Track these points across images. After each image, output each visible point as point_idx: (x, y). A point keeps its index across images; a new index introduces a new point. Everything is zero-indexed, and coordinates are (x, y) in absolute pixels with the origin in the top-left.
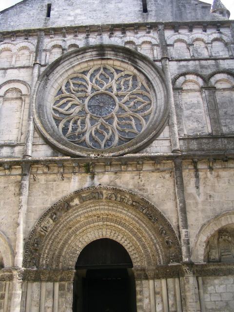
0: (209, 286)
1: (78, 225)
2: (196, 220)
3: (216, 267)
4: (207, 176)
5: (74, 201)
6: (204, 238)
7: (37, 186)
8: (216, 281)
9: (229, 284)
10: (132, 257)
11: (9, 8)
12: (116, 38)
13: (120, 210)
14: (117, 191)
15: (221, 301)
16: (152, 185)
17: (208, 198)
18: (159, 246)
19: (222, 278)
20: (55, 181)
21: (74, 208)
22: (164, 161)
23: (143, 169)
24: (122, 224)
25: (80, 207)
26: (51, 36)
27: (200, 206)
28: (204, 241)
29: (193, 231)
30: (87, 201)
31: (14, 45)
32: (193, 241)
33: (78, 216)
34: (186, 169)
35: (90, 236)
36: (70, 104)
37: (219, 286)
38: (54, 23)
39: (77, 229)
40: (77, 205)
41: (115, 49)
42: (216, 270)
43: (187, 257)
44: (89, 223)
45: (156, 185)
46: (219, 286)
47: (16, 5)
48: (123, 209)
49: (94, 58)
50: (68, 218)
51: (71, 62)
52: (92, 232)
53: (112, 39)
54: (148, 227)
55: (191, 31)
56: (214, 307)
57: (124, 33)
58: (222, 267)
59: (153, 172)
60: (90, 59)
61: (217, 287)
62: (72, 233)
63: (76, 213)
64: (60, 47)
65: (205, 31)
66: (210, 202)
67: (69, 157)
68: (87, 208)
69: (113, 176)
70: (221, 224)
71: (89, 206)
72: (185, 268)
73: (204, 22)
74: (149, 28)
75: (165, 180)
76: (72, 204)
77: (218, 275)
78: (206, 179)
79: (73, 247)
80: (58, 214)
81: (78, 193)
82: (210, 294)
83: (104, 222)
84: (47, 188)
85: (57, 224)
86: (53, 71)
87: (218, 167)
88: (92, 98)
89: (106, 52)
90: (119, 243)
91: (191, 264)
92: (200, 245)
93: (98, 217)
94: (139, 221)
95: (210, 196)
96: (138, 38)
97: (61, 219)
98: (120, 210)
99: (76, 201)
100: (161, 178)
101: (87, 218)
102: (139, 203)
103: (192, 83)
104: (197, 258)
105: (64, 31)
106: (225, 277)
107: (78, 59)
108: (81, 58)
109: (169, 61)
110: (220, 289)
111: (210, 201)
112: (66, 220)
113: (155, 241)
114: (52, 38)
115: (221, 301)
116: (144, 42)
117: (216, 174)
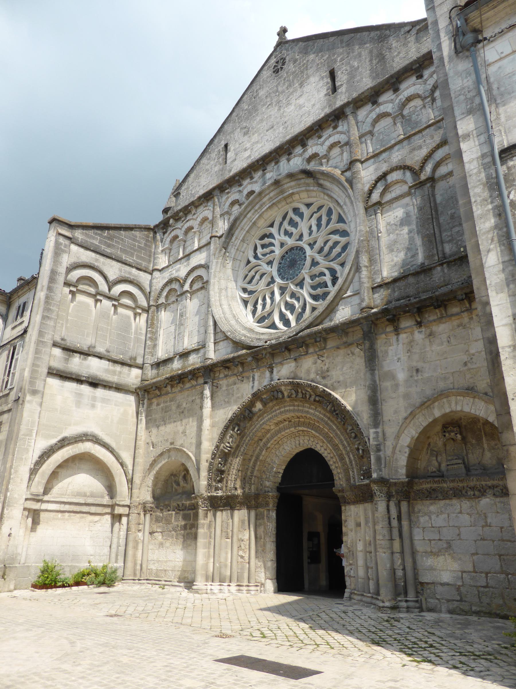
0: (422, 516)
1: (268, 435)
2: (396, 412)
3: (432, 485)
4: (413, 338)
5: (255, 407)
6: (406, 440)
7: (219, 394)
8: (432, 508)
9: (454, 513)
10: (334, 472)
11: (189, 172)
12: (296, 158)
13: (307, 409)
14: (296, 386)
15: (440, 540)
16: (338, 368)
17: (415, 374)
18: (353, 456)
19: (442, 503)
20: (235, 384)
21: (258, 414)
22: (351, 330)
23: (328, 347)
24: (315, 428)
25: (264, 413)
26: (226, 191)
27: (402, 390)
28: (406, 445)
29: (391, 430)
30: (269, 403)
31: (196, 220)
32: (391, 447)
33: (263, 423)
34: (382, 333)
35: (286, 448)
36: (257, 277)
37: (437, 516)
38: (230, 171)
39: (268, 441)
40: (260, 410)
41: (291, 176)
42: (433, 490)
43: (376, 471)
44: (279, 431)
45: (343, 368)
46: (437, 516)
47: (194, 165)
48: (309, 408)
49: (274, 201)
50: (254, 429)
51: (249, 219)
52: (288, 442)
53: (291, 162)
54: (339, 429)
55: (396, 90)
56: (429, 550)
57: (304, 145)
58: (441, 485)
59: (338, 348)
60: (270, 204)
61: (433, 517)
62: (263, 446)
63: (261, 420)
64: (404, 168)
65: (420, 77)
66: (416, 381)
67: (244, 351)
68: (272, 413)
69: (293, 364)
70: (434, 415)
71: (274, 409)
72: (375, 487)
73: (412, 64)
74: (333, 121)
75: (354, 357)
76: (255, 410)
77: (436, 498)
78: (412, 344)
79: (269, 464)
80: (242, 424)
81: (256, 396)
82: (424, 528)
83: (295, 427)
84: (228, 394)
85: (243, 437)
86: (231, 239)
87: (431, 318)
88: (283, 257)
89: (285, 186)
90: (324, 458)
91: (382, 481)
92: (400, 451)
93: (290, 421)
94: (329, 422)
95: (417, 371)
96: (322, 144)
97: (246, 431)
98: (307, 409)
99: (259, 406)
100: (349, 355)
101: (277, 424)
102: (323, 397)
103: (399, 184)
104: (397, 471)
105: (237, 178)
106: (447, 501)
107: (256, 211)
108: (259, 208)
109: (362, 163)
110: (439, 521)
111: (416, 378)
112: (252, 430)
113: (348, 448)
114: (228, 193)
115: (440, 540)
116: (332, 146)
117: (428, 331)
